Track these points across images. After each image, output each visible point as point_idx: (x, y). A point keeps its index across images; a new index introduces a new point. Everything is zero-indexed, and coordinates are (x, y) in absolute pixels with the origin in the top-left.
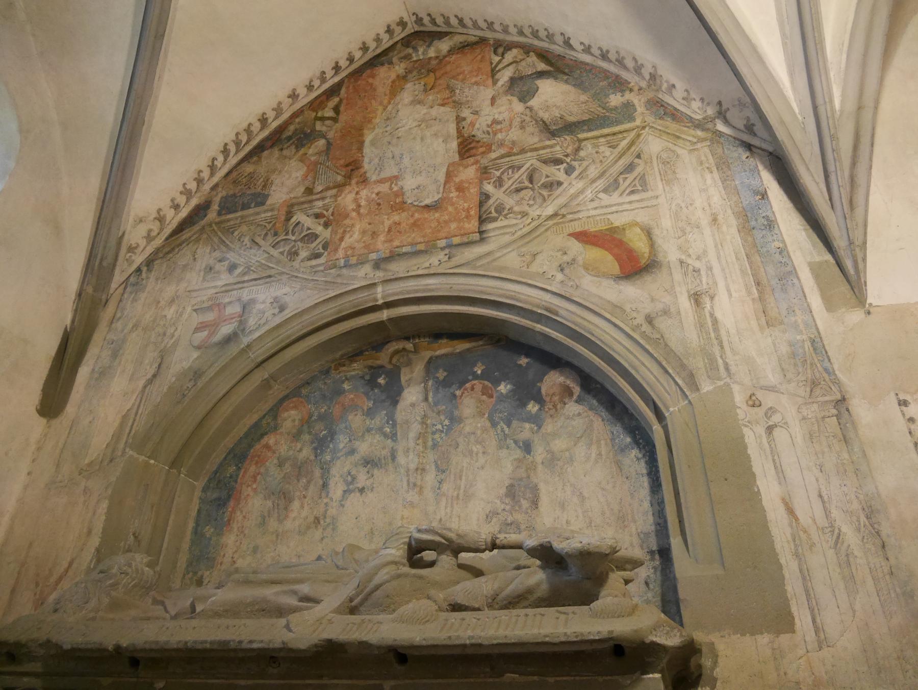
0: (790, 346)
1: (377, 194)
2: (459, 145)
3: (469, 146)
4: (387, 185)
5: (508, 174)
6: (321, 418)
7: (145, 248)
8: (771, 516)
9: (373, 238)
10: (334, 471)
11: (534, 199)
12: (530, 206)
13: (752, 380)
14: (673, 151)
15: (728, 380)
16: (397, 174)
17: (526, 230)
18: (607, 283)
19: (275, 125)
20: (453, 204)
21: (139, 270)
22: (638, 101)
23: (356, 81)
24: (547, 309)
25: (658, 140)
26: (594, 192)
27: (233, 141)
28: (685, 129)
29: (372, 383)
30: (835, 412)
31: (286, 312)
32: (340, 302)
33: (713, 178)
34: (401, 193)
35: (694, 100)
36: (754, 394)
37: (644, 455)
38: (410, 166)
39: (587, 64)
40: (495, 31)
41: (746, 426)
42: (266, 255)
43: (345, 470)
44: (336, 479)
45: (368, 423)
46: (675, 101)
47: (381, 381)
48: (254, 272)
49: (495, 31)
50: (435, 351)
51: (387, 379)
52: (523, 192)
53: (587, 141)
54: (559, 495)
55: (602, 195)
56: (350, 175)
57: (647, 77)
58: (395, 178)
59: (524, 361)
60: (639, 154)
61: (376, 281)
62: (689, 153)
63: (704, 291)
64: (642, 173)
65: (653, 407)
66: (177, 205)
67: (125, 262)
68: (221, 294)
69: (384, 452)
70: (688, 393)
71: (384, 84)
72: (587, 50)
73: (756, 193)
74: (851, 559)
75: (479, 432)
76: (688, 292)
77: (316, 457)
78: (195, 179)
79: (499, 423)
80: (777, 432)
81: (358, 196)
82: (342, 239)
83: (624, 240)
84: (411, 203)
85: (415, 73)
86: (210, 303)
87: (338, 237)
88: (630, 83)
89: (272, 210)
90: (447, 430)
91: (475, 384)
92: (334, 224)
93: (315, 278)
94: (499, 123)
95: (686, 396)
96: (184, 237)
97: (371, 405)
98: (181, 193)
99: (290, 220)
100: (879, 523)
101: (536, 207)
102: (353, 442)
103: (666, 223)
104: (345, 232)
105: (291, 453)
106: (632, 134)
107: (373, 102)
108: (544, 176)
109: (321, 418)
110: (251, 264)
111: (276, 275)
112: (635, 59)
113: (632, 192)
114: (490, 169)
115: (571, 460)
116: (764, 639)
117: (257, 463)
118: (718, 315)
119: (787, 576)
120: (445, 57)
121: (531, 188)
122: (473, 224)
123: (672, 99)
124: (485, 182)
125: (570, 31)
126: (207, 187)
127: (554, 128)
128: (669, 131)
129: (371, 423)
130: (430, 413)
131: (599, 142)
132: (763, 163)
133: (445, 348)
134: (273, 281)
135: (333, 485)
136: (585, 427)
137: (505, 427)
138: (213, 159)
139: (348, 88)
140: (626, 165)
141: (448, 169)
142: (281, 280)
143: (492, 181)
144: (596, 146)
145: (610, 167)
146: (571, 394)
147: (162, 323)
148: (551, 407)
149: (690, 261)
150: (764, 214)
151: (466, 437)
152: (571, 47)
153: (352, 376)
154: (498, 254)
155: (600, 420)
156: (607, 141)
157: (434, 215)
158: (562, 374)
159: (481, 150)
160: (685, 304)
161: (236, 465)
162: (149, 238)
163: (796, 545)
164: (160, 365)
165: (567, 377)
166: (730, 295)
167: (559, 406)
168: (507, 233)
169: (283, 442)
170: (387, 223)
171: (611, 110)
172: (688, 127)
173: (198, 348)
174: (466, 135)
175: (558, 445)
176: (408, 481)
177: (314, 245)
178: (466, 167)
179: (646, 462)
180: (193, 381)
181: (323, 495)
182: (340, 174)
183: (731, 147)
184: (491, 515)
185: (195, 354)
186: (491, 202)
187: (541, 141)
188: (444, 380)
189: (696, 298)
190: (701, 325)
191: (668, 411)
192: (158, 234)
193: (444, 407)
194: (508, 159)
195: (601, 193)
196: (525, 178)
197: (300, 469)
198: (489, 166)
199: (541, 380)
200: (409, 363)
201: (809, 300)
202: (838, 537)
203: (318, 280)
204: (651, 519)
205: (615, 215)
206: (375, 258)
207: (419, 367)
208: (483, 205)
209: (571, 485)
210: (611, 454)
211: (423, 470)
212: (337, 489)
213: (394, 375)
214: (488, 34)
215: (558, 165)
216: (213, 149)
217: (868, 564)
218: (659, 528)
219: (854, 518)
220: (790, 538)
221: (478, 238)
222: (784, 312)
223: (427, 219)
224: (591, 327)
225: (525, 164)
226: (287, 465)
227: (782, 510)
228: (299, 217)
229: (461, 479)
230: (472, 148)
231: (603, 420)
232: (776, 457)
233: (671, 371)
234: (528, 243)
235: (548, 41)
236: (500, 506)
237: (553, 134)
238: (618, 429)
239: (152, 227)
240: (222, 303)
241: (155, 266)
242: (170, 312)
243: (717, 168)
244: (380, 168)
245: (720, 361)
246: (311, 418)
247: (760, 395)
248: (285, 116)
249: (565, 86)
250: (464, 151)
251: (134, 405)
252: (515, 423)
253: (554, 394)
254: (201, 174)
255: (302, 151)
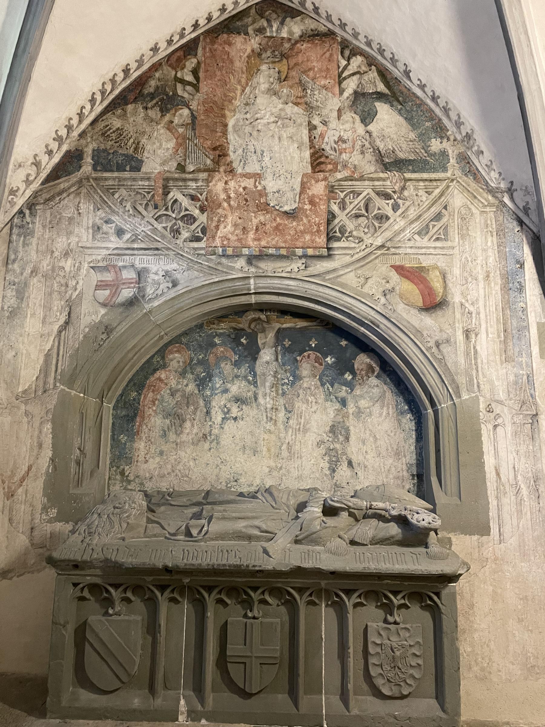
0: (515, 376)
1: (244, 188)
2: (312, 155)
3: (319, 160)
4: (252, 180)
5: (350, 198)
6: (201, 362)
7: (25, 191)
8: (488, 475)
9: (244, 233)
10: (214, 403)
11: (368, 228)
12: (366, 233)
13: (491, 395)
14: (470, 209)
15: (478, 393)
16: (259, 172)
17: (362, 254)
18: (414, 312)
19: (135, 75)
20: (307, 217)
21: (21, 212)
22: (452, 153)
23: (213, 43)
24: (372, 322)
25: (461, 195)
26: (411, 232)
27: (100, 91)
28: (481, 190)
29: (236, 340)
30: (531, 421)
31: (179, 287)
32: (221, 286)
33: (492, 241)
34: (263, 193)
35: (494, 170)
36: (490, 404)
37: (415, 419)
38: (271, 167)
39: (418, 97)
40: (345, 31)
41: (483, 423)
42: (150, 227)
43: (222, 403)
44: (216, 409)
45: (236, 371)
46: (480, 163)
47: (243, 340)
48: (142, 241)
49: (345, 31)
50: (282, 324)
51: (248, 340)
52: (361, 219)
53: (411, 182)
54: (362, 435)
55: (416, 237)
56: (218, 160)
57: (464, 134)
58: (257, 177)
59: (344, 343)
60: (446, 205)
61: (251, 276)
62: (480, 214)
63: (473, 329)
64: (446, 223)
65: (429, 398)
66: (51, 151)
67: (8, 203)
68: (115, 257)
69: (249, 394)
70: (454, 398)
71: (241, 57)
72: (422, 87)
73: (518, 262)
74: (522, 502)
75: (313, 388)
76: (463, 328)
77: (199, 391)
78: (66, 126)
79: (326, 384)
80: (499, 429)
81: (228, 187)
82: (217, 227)
83: (428, 278)
84: (273, 207)
85: (269, 53)
86: (105, 264)
87: (214, 224)
88: (448, 130)
89: (149, 179)
90: (291, 384)
91: (310, 354)
92: (209, 210)
93: (199, 261)
94: (344, 142)
95: (453, 400)
96: (62, 186)
97: (237, 358)
98: (54, 139)
99: (167, 195)
100: (539, 485)
101: (369, 235)
102: (226, 384)
103: (457, 271)
104: (219, 221)
105: (180, 386)
106: (444, 184)
107: (232, 77)
108: (377, 207)
109: (201, 362)
110: (137, 232)
111: (163, 249)
112: (459, 116)
113: (437, 239)
114: (336, 189)
115: (370, 415)
116: (475, 537)
117: (153, 391)
118: (478, 348)
119: (491, 508)
120: (297, 42)
121: (366, 217)
122: (321, 240)
123: (477, 161)
124: (332, 201)
125: (413, 66)
126: (75, 134)
127: (387, 160)
128: (469, 189)
129: (238, 372)
130: (279, 370)
131: (420, 186)
132: (527, 239)
133: (289, 323)
134: (162, 255)
135: (214, 413)
136: (380, 394)
137: (330, 386)
138: (82, 107)
139: (204, 48)
140: (436, 213)
141: (302, 180)
142: (169, 255)
143: (338, 201)
144: (416, 189)
145: (425, 212)
146: (373, 372)
147: (62, 274)
148: (360, 378)
149: (467, 305)
150: (519, 280)
151: (304, 390)
152: (409, 78)
153: (221, 333)
154: (341, 272)
155: (390, 392)
156: (425, 186)
157: (292, 223)
158: (369, 357)
159: (330, 167)
160: (460, 337)
161: (137, 392)
162: (28, 182)
163: (497, 492)
164: (69, 314)
165: (372, 359)
166: (488, 335)
167: (365, 378)
168: (348, 254)
169: (172, 377)
170: (255, 221)
171: (432, 155)
172: (483, 189)
173: (104, 305)
174: (317, 147)
175: (363, 403)
176: (267, 416)
177: (193, 227)
178: (317, 181)
179: (415, 423)
180: (106, 334)
181: (208, 419)
182: (209, 158)
183: (510, 219)
184: (320, 443)
185: (103, 311)
186: (336, 221)
187: (376, 171)
188: (289, 347)
189: (467, 333)
190: (468, 354)
191: (440, 405)
192: (36, 178)
193: (289, 367)
194: (350, 183)
195: (416, 235)
196: (362, 205)
197: (188, 399)
198: (334, 186)
199: (355, 359)
200: (263, 331)
201: (532, 348)
202: (518, 490)
203: (202, 264)
204: (414, 457)
205: (423, 256)
206: (247, 253)
207: (271, 335)
208: (330, 223)
209: (369, 430)
210: (395, 414)
211: (277, 409)
212: (218, 417)
213: (253, 338)
214: (338, 30)
215: (388, 200)
216: (83, 99)
217: (530, 505)
218: (418, 462)
219: (528, 481)
220: (495, 488)
221: (326, 254)
222: (516, 354)
223: (286, 225)
224: (400, 341)
225: (363, 191)
226: (177, 395)
227: (494, 473)
228: (175, 194)
229: (301, 418)
230: (322, 163)
231: (392, 392)
232: (496, 444)
233: (446, 383)
234: (363, 266)
235: (390, 62)
236: (326, 438)
237: (386, 167)
238: (400, 399)
239: (30, 172)
240: (117, 265)
241: (38, 211)
242: (68, 264)
243: (497, 234)
244: (244, 161)
245: (475, 381)
246: (192, 362)
247: (493, 405)
248: (145, 67)
249: (398, 117)
250: (315, 163)
251: (53, 346)
252: (336, 385)
253: (362, 370)
254: (71, 121)
255: (167, 117)
